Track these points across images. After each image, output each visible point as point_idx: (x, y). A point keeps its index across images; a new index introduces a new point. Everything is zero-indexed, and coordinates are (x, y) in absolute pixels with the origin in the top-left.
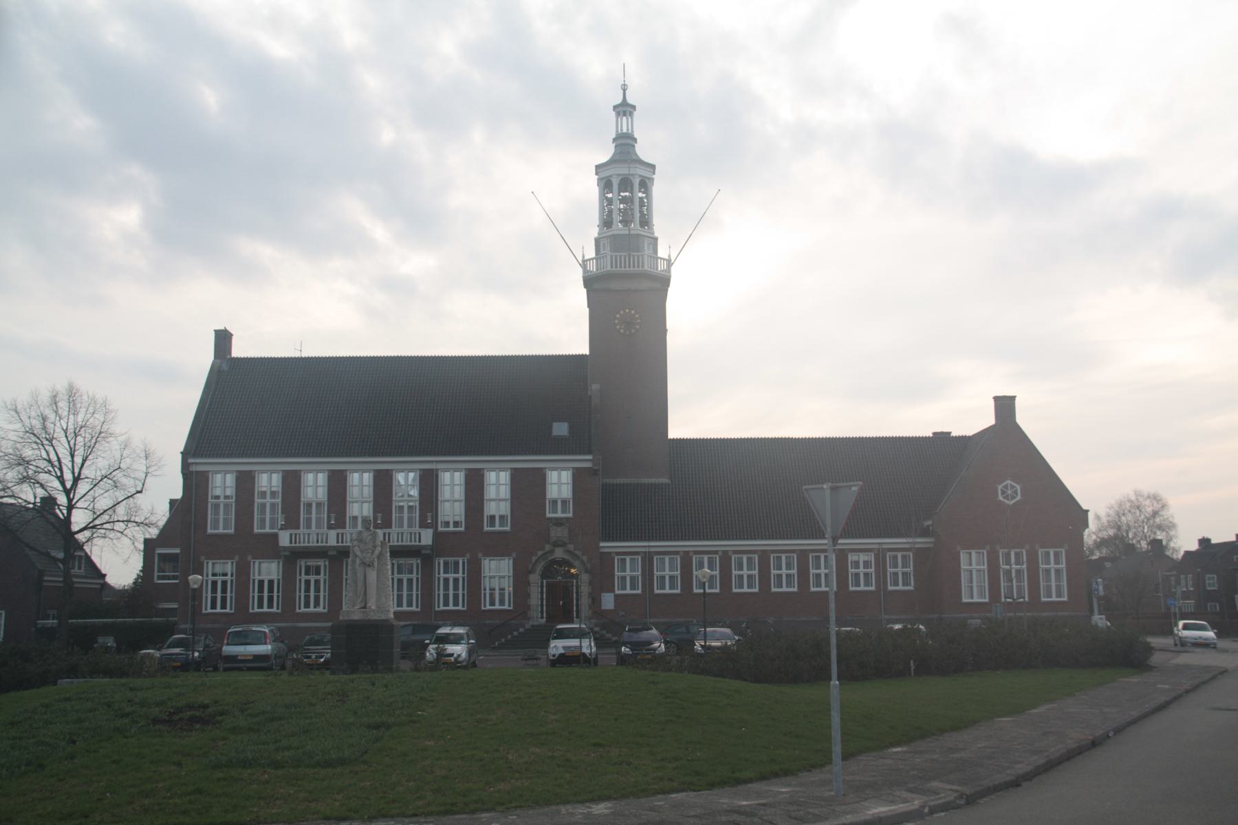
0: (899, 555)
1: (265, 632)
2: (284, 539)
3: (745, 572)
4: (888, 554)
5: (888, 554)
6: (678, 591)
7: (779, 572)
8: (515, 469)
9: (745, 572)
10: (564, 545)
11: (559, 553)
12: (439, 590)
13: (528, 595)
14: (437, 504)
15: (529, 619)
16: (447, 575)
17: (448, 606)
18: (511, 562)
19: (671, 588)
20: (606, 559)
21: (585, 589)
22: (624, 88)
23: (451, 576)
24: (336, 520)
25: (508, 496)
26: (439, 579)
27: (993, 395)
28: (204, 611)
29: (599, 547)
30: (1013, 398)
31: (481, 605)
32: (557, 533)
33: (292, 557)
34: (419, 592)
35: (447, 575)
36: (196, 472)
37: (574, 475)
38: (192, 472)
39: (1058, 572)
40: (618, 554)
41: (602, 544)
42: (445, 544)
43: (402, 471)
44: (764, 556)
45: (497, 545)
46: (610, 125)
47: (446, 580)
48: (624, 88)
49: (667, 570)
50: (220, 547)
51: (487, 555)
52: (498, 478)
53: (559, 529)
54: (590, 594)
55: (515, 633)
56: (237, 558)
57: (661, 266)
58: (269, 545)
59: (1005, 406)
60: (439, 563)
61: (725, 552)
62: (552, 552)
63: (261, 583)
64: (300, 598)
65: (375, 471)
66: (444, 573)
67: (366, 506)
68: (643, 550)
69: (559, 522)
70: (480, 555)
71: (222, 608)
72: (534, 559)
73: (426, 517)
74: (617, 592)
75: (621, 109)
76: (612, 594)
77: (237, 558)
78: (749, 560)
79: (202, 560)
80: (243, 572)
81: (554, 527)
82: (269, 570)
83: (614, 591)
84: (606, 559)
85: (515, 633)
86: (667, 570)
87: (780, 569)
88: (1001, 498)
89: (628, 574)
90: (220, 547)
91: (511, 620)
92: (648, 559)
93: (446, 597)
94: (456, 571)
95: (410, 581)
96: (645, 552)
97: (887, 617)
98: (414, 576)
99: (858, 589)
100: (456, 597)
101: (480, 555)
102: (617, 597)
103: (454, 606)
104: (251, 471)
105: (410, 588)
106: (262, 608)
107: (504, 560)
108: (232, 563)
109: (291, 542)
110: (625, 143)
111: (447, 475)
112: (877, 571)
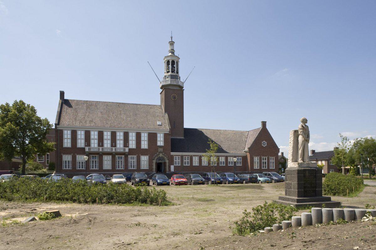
0: (187, 157)
1: (260, 177)
2: (87, 149)
3: (187, 161)
6: (189, 165)
7: (176, 161)
8: (73, 130)
9: (187, 161)
10: (162, 153)
11: (161, 155)
13: (153, 166)
15: (153, 172)
18: (71, 156)
19: (187, 164)
20: (172, 157)
21: (167, 164)
22: (172, 43)
23: (132, 160)
25: (70, 138)
27: (262, 121)
29: (170, 154)
32: (161, 150)
33: (88, 154)
37: (72, 132)
39: (273, 162)
40: (194, 156)
41: (171, 153)
42: (131, 151)
43: (106, 131)
44: (182, 157)
45: (144, 152)
46: (169, 48)
47: (131, 161)
48: (172, 43)
50: (68, 151)
51: (142, 155)
52: (107, 134)
53: (161, 149)
54: (168, 165)
55: (149, 175)
56: (72, 154)
57: (180, 84)
58: (82, 151)
60: (91, 156)
61: (191, 156)
62: (159, 154)
63: (66, 162)
65: (136, 132)
66: (131, 159)
67: (162, 142)
68: (181, 155)
69: (161, 147)
70: (140, 155)
71: (68, 168)
72: (154, 156)
74: (175, 165)
75: (171, 43)
76: (173, 166)
77: (72, 154)
78: (188, 157)
80: (74, 159)
84: (172, 157)
85: (149, 175)
86: (187, 161)
88: (262, 145)
90: (68, 151)
93: (93, 166)
94: (96, 159)
95: (96, 161)
96: (200, 156)
98: (135, 160)
99: (176, 165)
101: (140, 155)
105: (96, 163)
106: (80, 168)
108: (258, 158)
109: (89, 150)
110: (172, 52)
111: (131, 133)
112: (183, 161)
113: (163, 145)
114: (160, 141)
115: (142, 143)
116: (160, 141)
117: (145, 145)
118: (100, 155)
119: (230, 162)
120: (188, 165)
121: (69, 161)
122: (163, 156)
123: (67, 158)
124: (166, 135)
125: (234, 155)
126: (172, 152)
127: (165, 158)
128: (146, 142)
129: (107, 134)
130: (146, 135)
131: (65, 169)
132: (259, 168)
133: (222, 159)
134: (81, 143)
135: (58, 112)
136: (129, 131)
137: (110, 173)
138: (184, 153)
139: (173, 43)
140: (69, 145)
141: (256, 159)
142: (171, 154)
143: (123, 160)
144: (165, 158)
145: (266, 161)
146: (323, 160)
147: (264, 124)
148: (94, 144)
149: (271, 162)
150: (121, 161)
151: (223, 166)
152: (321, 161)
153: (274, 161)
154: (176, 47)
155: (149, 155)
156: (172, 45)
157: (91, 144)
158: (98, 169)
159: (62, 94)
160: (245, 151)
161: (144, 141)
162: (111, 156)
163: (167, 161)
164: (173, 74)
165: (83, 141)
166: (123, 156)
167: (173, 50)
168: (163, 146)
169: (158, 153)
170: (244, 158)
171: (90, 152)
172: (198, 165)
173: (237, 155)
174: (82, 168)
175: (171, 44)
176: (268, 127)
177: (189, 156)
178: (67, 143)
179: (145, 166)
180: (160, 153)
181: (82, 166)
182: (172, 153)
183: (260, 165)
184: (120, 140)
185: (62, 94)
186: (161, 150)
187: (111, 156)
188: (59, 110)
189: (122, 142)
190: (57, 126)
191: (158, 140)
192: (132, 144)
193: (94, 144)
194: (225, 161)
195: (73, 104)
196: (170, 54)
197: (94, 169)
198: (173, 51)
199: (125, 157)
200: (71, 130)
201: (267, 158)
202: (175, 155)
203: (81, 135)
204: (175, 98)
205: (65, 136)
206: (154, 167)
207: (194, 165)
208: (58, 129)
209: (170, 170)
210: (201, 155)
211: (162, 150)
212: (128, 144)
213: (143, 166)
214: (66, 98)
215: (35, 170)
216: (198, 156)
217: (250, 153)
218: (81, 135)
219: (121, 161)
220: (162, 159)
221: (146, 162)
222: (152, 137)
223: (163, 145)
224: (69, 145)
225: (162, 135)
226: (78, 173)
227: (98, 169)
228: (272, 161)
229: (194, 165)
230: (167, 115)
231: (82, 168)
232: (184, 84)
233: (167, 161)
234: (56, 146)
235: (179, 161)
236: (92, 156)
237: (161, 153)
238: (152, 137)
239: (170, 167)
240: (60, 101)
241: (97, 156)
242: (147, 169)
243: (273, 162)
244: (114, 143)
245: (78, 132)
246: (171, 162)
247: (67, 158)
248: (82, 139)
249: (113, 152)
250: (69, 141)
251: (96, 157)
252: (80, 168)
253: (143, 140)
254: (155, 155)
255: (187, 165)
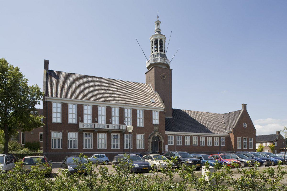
0: (179, 136)
1: (6, 157)
4: (177, 136)
5: (177, 136)
10: (158, 132)
11: (157, 134)
12: (61, 144)
14: (124, 118)
16: (127, 139)
17: (56, 147)
19: (203, 145)
21: (163, 144)
22: (158, 23)
24: (109, 120)
26: (125, 140)
28: (52, 148)
29: (165, 133)
30: (246, 104)
31: (51, 147)
32: (156, 128)
34: (62, 143)
35: (127, 139)
36: (48, 102)
38: (46, 101)
40: (193, 136)
41: (166, 132)
44: (175, 136)
48: (158, 23)
49: (202, 139)
50: (57, 127)
52: (73, 107)
56: (63, 131)
58: (75, 128)
59: (245, 106)
60: (84, 134)
61: (183, 135)
62: (155, 133)
64: (125, 145)
68: (174, 134)
69: (156, 125)
70: (136, 133)
72: (150, 135)
73: (79, 119)
74: (169, 145)
77: (63, 131)
79: (67, 132)
80: (65, 136)
81: (155, 127)
82: (73, 136)
83: (168, 145)
84: (166, 135)
87: (170, 139)
89: (171, 140)
90: (57, 127)
91: (145, 152)
92: (199, 137)
96: (175, 135)
97: (221, 152)
99: (170, 145)
100: (89, 145)
102: (168, 146)
103: (74, 147)
104: (82, 104)
107: (189, 140)
110: (159, 31)
111: (86, 107)
113: (158, 124)
114: (156, 120)
115: (70, 116)
116: (156, 120)
117: (140, 123)
118: (95, 132)
119: (209, 142)
120: (203, 145)
121: (56, 139)
122: (158, 135)
123: (56, 135)
124: (160, 113)
125: (219, 136)
126: (166, 130)
127: (161, 137)
128: (141, 120)
129: (73, 107)
130: (142, 112)
131: (54, 148)
132: (241, 148)
133: (210, 140)
134: (72, 119)
135: (44, 82)
136: (124, 107)
137: (89, 153)
138: (177, 132)
139: (159, 22)
140: (59, 121)
141: (239, 140)
142: (166, 134)
143: (119, 139)
144: (161, 137)
145: (181, 140)
146: (268, 142)
147: (245, 106)
148: (88, 120)
149: (239, 142)
150: (89, 140)
151: (171, 146)
152: (266, 142)
153: (252, 142)
154: (162, 27)
155: (145, 134)
156: (159, 24)
157: (84, 120)
158: (92, 148)
159: (46, 63)
160: (227, 132)
161: (72, 114)
162: (106, 134)
163: (163, 141)
164: (156, 52)
165: (75, 116)
166: (119, 134)
167: (159, 29)
168: (158, 125)
169: (153, 132)
170: (228, 139)
171: (84, 128)
172: (190, 145)
173: (221, 136)
174: (74, 147)
175: (157, 23)
176: (248, 109)
177: (181, 135)
178: (57, 118)
179: (103, 145)
180: (155, 131)
181: (75, 144)
182: (167, 133)
183: (242, 145)
184: (87, 115)
185: (46, 63)
186: (156, 129)
187: (106, 134)
188: (45, 80)
189: (90, 117)
190: (46, 97)
191: (125, 116)
192: (73, 118)
193: (88, 120)
194: (211, 141)
195: (59, 76)
196: (157, 33)
197: (88, 148)
198: (159, 30)
199: (121, 136)
200: (77, 104)
201: (247, 138)
202: (169, 135)
203: (73, 110)
204: (164, 77)
205: (54, 110)
206: (150, 146)
207: (185, 145)
208: (46, 100)
209: (165, 150)
210: (176, 134)
211: (158, 129)
212: (96, 119)
213: (100, 145)
214: (50, 68)
215: (13, 150)
216: (189, 135)
217: (233, 134)
218: (57, 108)
219: (89, 140)
220: (158, 138)
221: (103, 140)
222: (148, 114)
223: (158, 124)
224: (59, 121)
225: (157, 113)
226: (70, 153)
227: (106, 148)
228: (179, 140)
229: (185, 145)
230: (157, 93)
231: (59, 147)
232: (171, 63)
233: (163, 141)
234: (44, 120)
235: (170, 140)
236: (85, 133)
237: (157, 132)
238: (148, 114)
239: (164, 147)
240: (44, 71)
241: (91, 133)
242: (105, 148)
243: (246, 142)
244: (80, 118)
245: (69, 105)
246: (166, 143)
247: (56, 135)
248: (59, 113)
249: (124, 130)
250: (59, 115)
251: (90, 134)
252: (117, 147)
253: (59, 113)
254: (151, 134)
255: (179, 145)
